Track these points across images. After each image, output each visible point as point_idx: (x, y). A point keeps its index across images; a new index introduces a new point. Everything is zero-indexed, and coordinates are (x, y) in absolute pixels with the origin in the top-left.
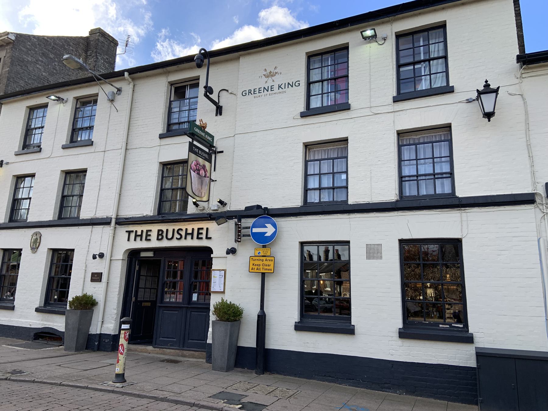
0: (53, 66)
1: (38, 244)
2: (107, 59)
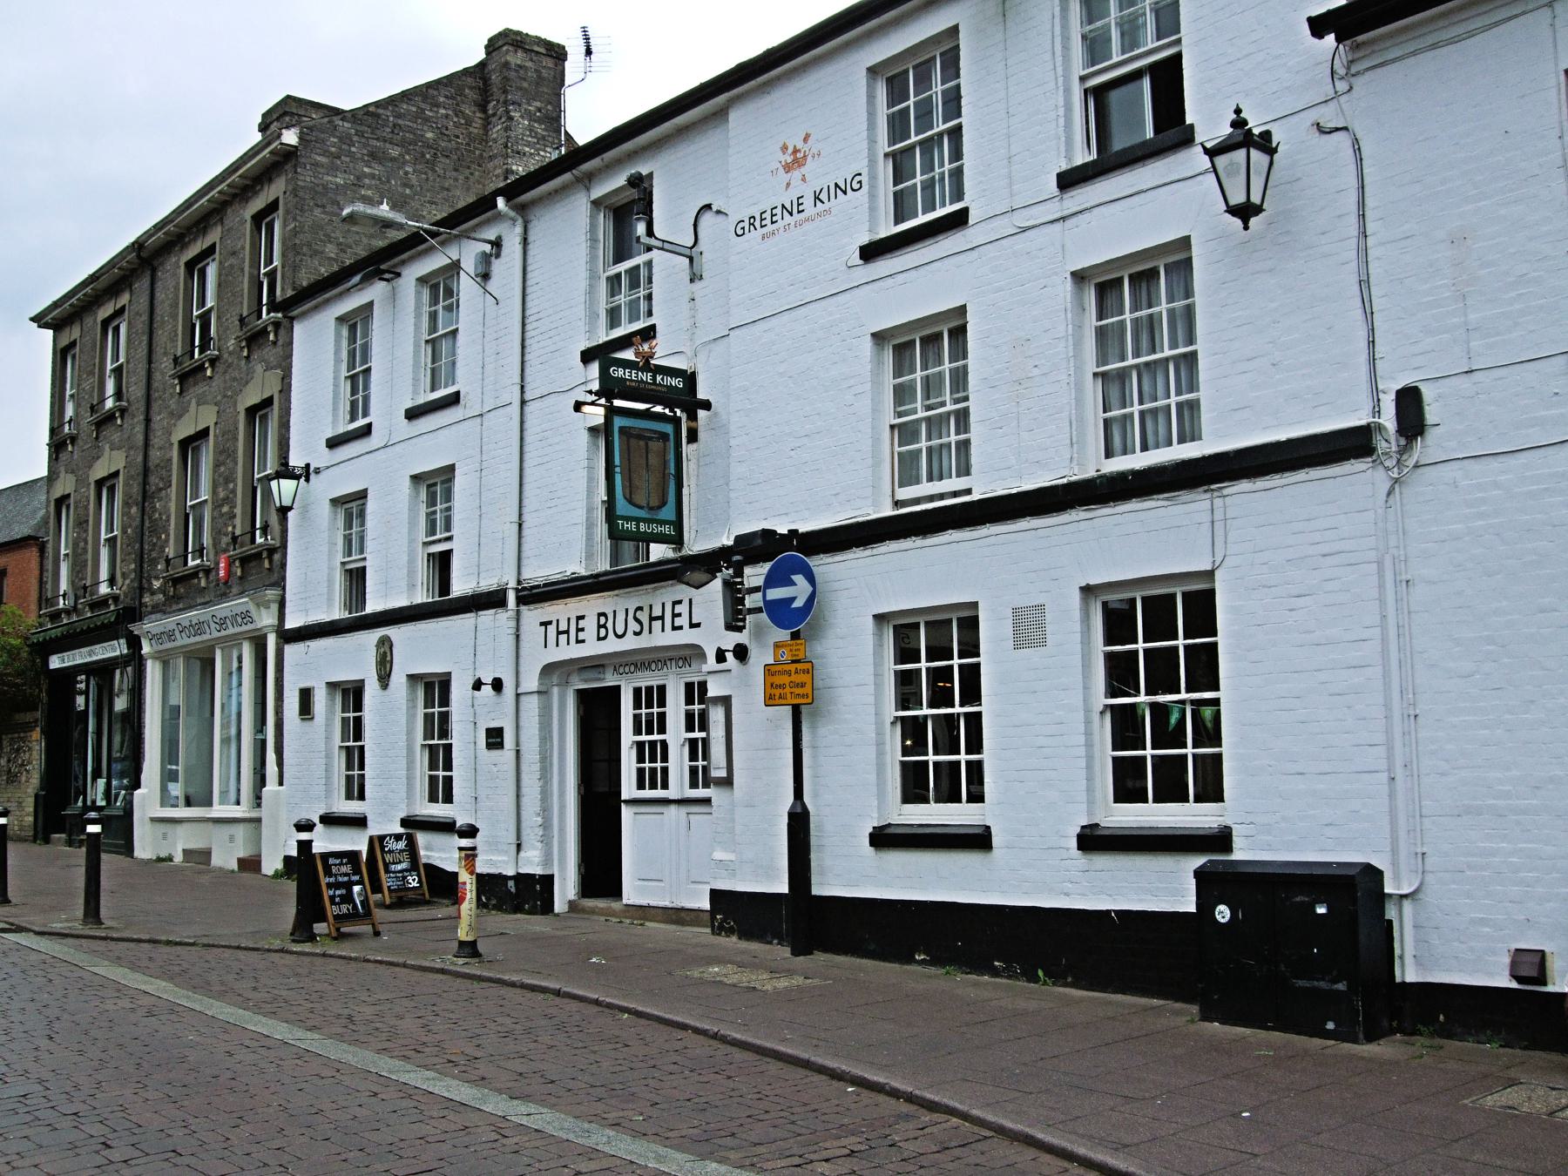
0: (401, 178)
1: (388, 666)
2: (540, 110)
